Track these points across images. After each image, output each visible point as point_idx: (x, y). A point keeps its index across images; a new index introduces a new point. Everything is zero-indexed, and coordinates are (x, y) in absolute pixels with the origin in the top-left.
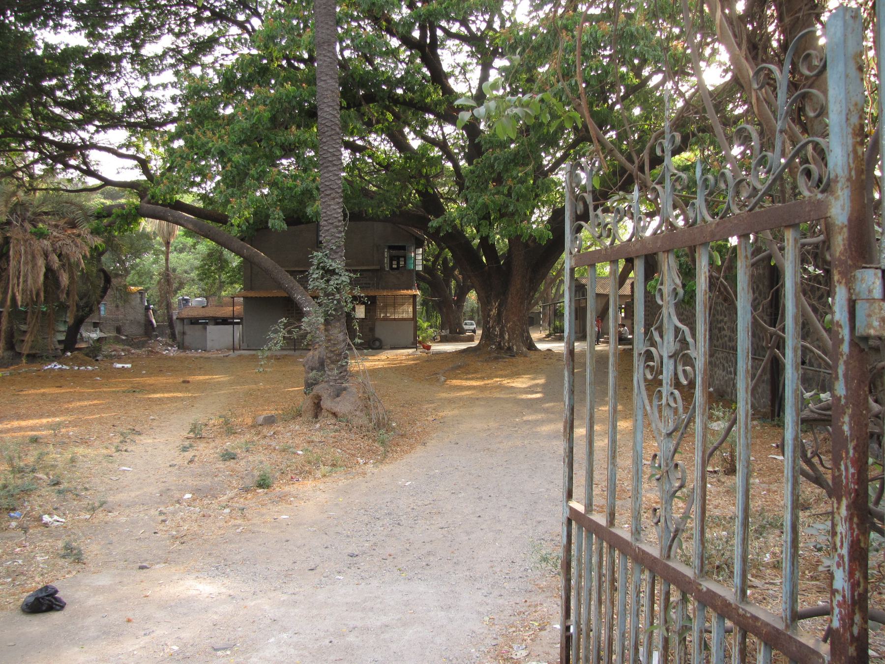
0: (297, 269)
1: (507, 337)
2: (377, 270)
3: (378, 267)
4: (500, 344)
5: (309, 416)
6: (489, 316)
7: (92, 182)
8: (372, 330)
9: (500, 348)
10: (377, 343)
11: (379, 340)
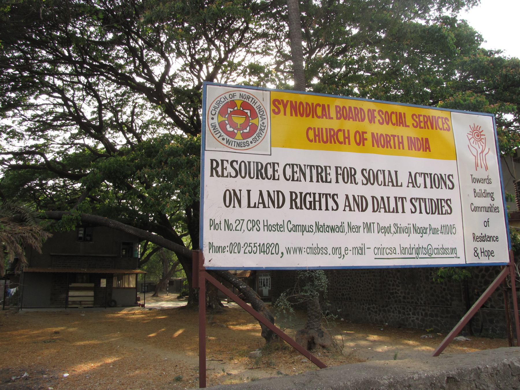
0: (64, 254)
10: (113, 303)
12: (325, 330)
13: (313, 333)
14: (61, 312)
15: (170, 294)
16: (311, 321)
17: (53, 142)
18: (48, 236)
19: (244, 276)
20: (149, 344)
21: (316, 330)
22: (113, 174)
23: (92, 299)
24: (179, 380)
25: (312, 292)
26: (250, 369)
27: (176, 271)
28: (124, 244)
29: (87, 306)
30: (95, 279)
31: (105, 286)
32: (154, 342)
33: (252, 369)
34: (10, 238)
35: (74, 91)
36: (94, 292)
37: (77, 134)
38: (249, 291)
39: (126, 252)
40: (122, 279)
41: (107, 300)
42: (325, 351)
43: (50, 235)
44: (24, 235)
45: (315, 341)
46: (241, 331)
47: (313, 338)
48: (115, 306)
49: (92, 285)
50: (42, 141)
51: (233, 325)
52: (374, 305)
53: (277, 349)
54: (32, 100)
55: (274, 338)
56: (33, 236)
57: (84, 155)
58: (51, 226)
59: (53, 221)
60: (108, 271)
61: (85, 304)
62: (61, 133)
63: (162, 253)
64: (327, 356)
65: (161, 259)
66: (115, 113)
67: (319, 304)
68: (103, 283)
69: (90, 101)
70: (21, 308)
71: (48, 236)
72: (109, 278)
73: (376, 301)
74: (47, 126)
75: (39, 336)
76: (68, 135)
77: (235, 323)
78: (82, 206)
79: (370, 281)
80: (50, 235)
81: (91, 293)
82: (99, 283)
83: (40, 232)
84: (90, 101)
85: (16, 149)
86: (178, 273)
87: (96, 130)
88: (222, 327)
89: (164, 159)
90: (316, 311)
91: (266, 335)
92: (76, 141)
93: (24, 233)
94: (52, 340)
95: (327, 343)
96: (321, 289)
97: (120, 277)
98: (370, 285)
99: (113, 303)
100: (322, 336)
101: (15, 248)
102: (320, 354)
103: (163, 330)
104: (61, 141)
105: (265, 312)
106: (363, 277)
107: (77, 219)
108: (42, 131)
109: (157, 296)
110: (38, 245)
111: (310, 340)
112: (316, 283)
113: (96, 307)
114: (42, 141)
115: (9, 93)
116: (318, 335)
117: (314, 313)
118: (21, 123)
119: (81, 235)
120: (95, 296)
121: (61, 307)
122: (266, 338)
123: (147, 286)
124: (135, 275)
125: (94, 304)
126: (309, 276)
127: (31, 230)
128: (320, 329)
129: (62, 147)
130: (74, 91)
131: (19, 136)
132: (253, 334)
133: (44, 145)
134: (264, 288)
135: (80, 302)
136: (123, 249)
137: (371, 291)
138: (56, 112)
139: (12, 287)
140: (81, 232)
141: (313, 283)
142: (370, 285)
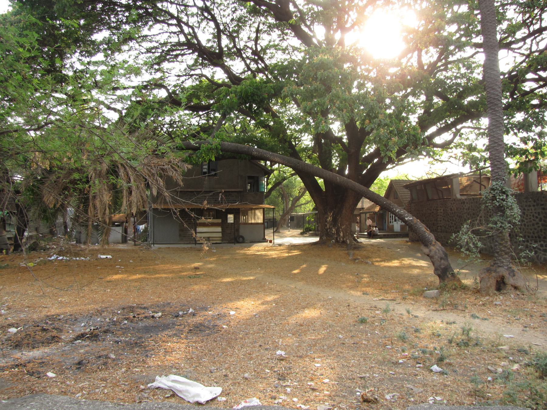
0: (190, 190)
1: (341, 234)
2: (240, 192)
3: (242, 190)
4: (337, 238)
5: (493, 290)
6: (326, 221)
7: (248, 61)
8: (238, 230)
9: (337, 241)
10: (241, 239)
11: (242, 237)
12: (515, 268)
13: (503, 271)
14: (191, 248)
15: (291, 230)
16: (500, 258)
17: (169, 75)
18: (187, 167)
19: (372, 210)
20: (299, 281)
21: (506, 268)
22: (250, 98)
23: (220, 235)
24: (364, 323)
25: (502, 223)
26: (434, 311)
27: (297, 206)
28: (250, 177)
29: (215, 242)
30: (221, 215)
31: (232, 222)
32: (302, 279)
33: (436, 310)
34: (150, 171)
35: (188, 17)
36: (222, 228)
37: (193, 65)
38: (416, 223)
39: (251, 186)
40: (247, 214)
41: (235, 236)
42: (518, 292)
43: (190, 167)
44: (164, 167)
45: (506, 281)
46: (390, 267)
47: (503, 278)
48: (243, 242)
49: (219, 221)
50: (159, 75)
51: (377, 261)
52: (542, 243)
53: (455, 289)
54: (145, 31)
55: (449, 276)
56: (173, 168)
57: (201, 87)
58: (189, 157)
59: (190, 152)
60: (236, 205)
61: (213, 240)
62: (175, 65)
63: (281, 188)
64: (522, 299)
65: (280, 194)
66: (232, 38)
67: (509, 238)
68: (231, 218)
69: (205, 28)
70: (154, 244)
71: (187, 167)
72: (237, 213)
73: (545, 238)
74: (161, 59)
75: (181, 272)
76: (184, 66)
77: (378, 259)
78: (219, 134)
79: (537, 215)
80: (190, 167)
81: (219, 229)
82: (226, 219)
83: (179, 164)
84: (205, 28)
85: (135, 84)
86: (298, 208)
87: (213, 57)
88: (367, 263)
89: (312, 74)
90: (505, 247)
91: (439, 273)
92: (192, 72)
93: (164, 165)
94: (196, 276)
95: (520, 283)
96: (514, 221)
97: (245, 213)
98: (537, 220)
99: (241, 239)
100: (514, 276)
101: (157, 181)
102: (512, 296)
103: (304, 266)
104: (179, 73)
105: (438, 247)
106: (528, 210)
107: (217, 148)
108: (158, 64)
109: (279, 232)
110: (177, 177)
111: (499, 280)
112: (508, 212)
113: (224, 243)
114: (159, 75)
115: (124, 25)
116: (509, 274)
117: (503, 249)
118: (137, 57)
119: (205, 170)
120: (223, 232)
121: (190, 243)
122: (439, 276)
123: (267, 222)
124: (262, 210)
125: (222, 240)
126: (500, 205)
127: (170, 162)
128: (510, 268)
129: (179, 80)
130: (188, 17)
131: (137, 72)
132: (405, 271)
133: (161, 79)
134: (395, 223)
135: (209, 238)
136: (249, 183)
137: (539, 227)
138: (171, 43)
139: (141, 224)
140: (205, 167)
141: (504, 213)
142: (537, 220)
